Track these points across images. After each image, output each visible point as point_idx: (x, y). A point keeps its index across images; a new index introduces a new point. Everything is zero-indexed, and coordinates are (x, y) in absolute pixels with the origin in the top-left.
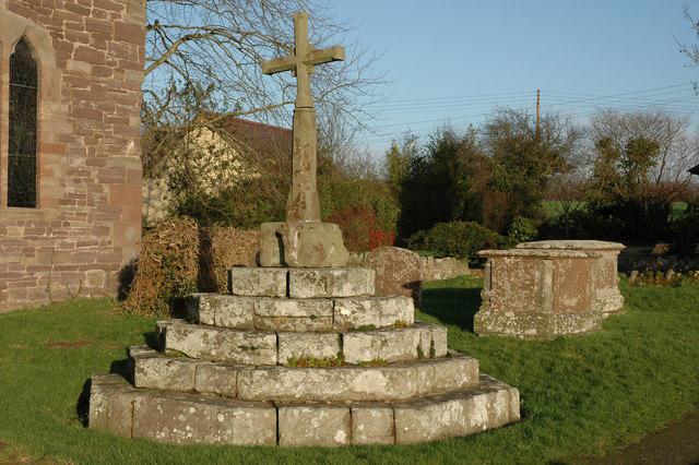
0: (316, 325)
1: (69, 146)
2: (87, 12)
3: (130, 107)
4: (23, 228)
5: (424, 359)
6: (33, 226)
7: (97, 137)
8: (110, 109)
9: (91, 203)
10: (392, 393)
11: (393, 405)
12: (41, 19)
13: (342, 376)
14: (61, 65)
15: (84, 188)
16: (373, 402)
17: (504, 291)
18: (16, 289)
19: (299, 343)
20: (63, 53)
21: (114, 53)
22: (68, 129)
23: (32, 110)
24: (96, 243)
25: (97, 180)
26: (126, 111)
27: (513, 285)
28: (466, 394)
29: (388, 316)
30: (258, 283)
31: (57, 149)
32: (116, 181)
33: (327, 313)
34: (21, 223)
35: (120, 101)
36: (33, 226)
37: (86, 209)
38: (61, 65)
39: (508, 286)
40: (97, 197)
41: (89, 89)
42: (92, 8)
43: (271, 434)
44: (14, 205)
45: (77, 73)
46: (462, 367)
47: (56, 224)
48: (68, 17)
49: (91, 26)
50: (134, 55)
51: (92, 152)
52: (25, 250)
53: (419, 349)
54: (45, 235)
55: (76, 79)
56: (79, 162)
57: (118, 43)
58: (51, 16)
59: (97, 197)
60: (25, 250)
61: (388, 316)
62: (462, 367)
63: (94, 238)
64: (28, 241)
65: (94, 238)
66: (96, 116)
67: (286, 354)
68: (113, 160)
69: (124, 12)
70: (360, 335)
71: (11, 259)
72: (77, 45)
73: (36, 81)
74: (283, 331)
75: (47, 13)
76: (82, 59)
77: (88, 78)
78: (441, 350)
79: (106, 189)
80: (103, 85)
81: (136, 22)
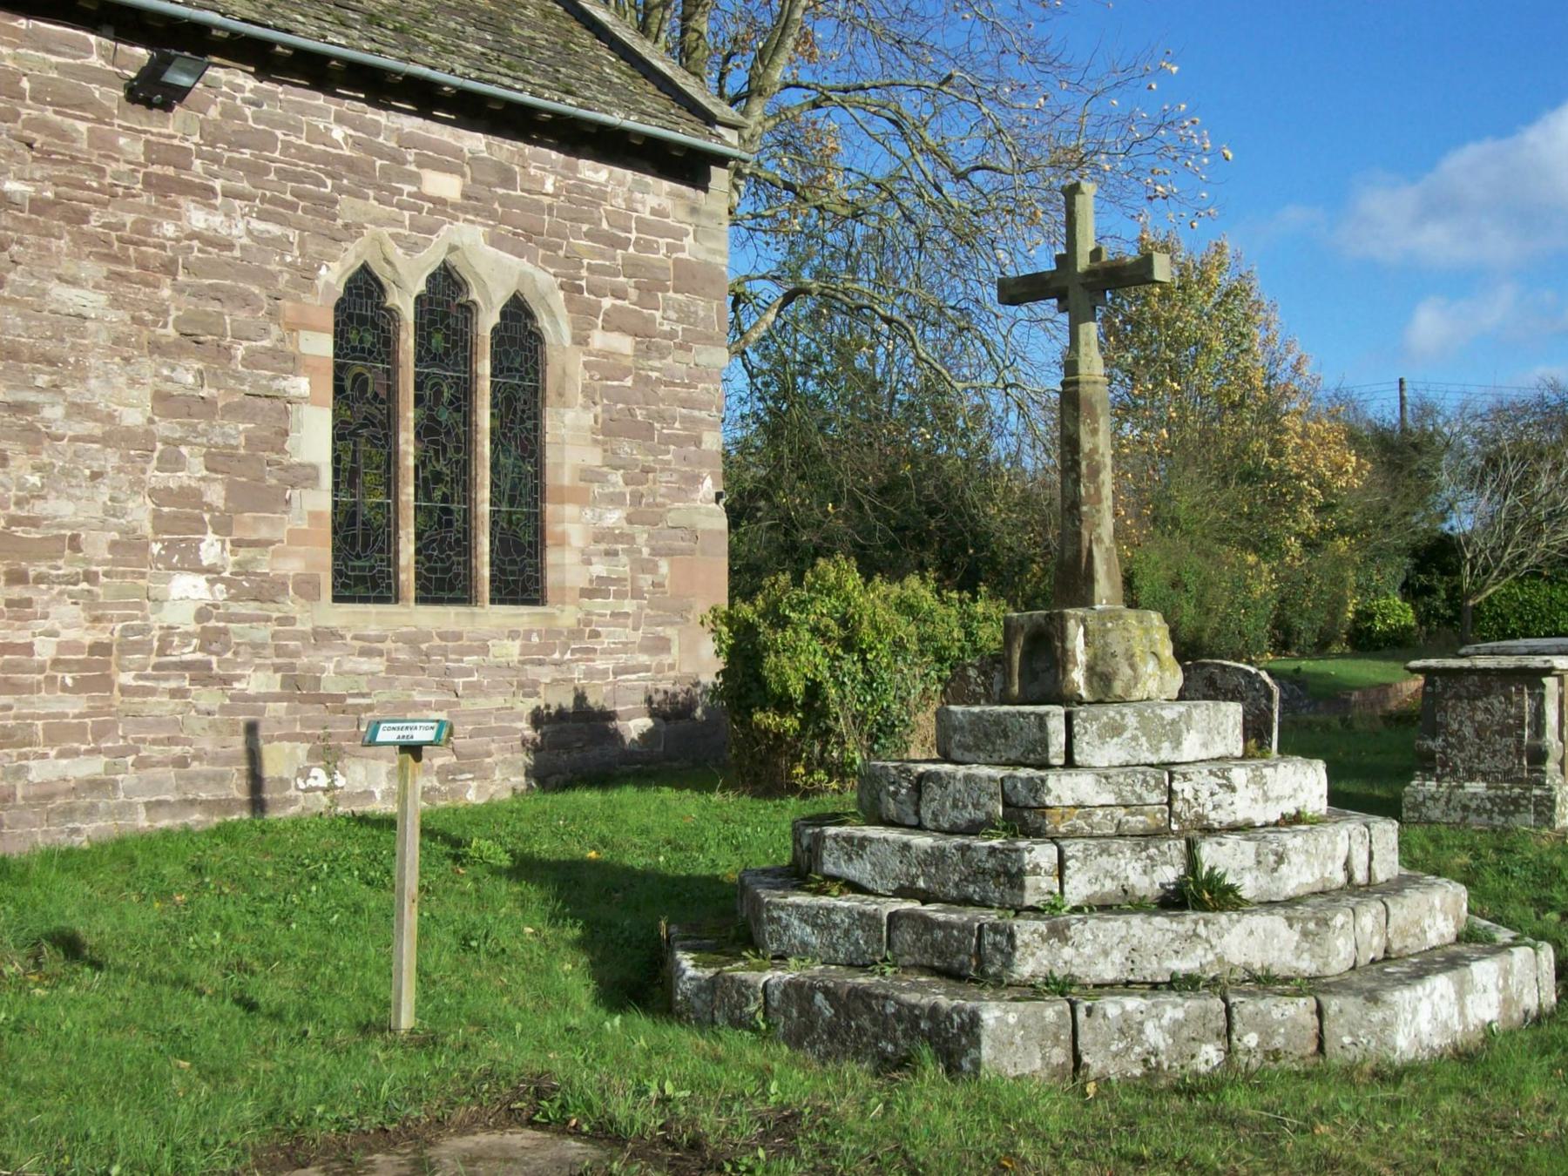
0: (1137, 822)
1: (596, 488)
2: (624, 243)
3: (704, 414)
4: (518, 643)
5: (1357, 890)
6: (535, 639)
7: (646, 470)
8: (667, 420)
9: (637, 594)
10: (1307, 965)
11: (1314, 986)
12: (546, 260)
13: (1201, 929)
14: (581, 340)
15: (623, 567)
16: (1265, 982)
17: (1462, 739)
18: (508, 755)
19: (1104, 861)
20: (584, 316)
21: (673, 316)
22: (594, 458)
23: (529, 424)
24: (647, 669)
25: (646, 551)
26: (695, 421)
27: (1479, 731)
28: (1449, 960)
29: (1279, 799)
30: (1006, 737)
31: (582, 499)
32: (682, 552)
33: (1156, 797)
34: (513, 635)
35: (684, 403)
36: (535, 639)
37: (629, 606)
38: (581, 340)
39: (1468, 731)
40: (645, 581)
41: (1175, 69)
42: (633, 236)
43: (237, 789)
44: (502, 602)
45: (607, 354)
46: (1437, 903)
47: (575, 634)
48: (593, 253)
49: (632, 269)
50: (708, 317)
51: (637, 498)
52: (521, 685)
53: (1347, 866)
54: (557, 656)
55: (606, 366)
56: (614, 517)
57: (679, 296)
58: (561, 253)
59: (645, 581)
60: (521, 685)
61: (1279, 799)
62: (1437, 903)
63: (644, 659)
64: (528, 667)
65: (644, 659)
66: (642, 432)
67: (1078, 888)
68: (677, 512)
69: (688, 241)
70: (1231, 839)
71: (498, 701)
72: (607, 302)
73: (536, 373)
74: (1065, 837)
75: (555, 248)
76: (619, 329)
77: (628, 362)
78: (1388, 866)
79: (664, 566)
80: (654, 375)
81: (710, 258)
